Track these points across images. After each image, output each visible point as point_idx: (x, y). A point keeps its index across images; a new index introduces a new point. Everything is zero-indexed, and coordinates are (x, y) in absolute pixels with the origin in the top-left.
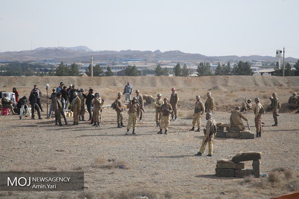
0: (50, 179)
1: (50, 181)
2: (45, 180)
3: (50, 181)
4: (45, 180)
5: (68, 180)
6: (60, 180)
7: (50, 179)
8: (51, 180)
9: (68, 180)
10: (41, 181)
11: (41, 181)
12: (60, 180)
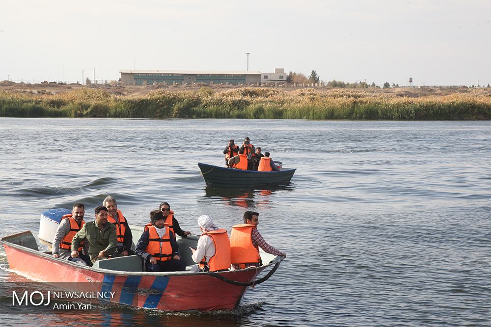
0: (82, 295)
1: (82, 297)
2: (74, 295)
3: (82, 297)
4: (74, 295)
5: (112, 295)
6: (57, 294)
7: (82, 295)
8: (84, 296)
9: (112, 295)
10: (68, 297)
11: (68, 297)
12: (57, 294)
